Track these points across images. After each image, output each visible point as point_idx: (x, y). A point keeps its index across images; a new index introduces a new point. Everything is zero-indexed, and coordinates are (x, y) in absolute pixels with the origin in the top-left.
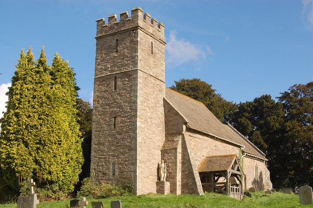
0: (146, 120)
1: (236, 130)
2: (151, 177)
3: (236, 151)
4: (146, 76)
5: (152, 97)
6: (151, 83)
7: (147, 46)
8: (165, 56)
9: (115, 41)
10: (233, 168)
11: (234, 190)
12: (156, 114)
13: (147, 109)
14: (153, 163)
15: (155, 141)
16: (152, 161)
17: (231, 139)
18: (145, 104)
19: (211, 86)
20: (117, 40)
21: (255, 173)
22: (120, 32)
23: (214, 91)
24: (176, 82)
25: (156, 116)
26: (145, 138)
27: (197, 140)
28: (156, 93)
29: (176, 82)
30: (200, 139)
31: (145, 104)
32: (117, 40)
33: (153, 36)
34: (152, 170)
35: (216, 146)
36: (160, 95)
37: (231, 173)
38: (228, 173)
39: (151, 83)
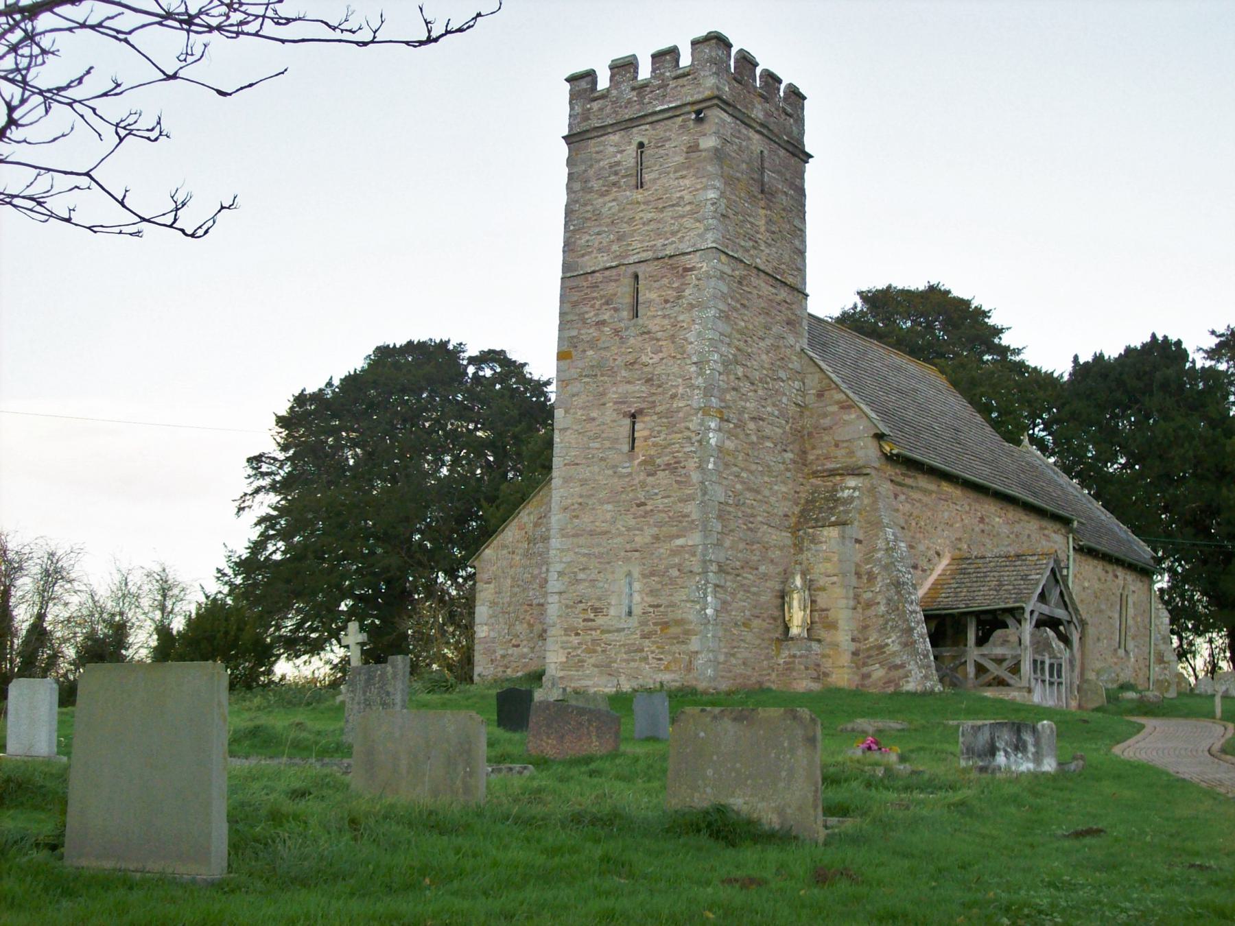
0: (741, 425)
1: (875, 342)
2: (756, 623)
3: (1057, 542)
4: (1148, 657)
5: (761, 344)
6: (760, 297)
7: (744, 166)
8: (325, 533)
9: (632, 149)
10: (1042, 597)
11: (1043, 669)
12: (774, 405)
13: (745, 387)
14: (765, 575)
15: (772, 500)
16: (762, 569)
17: (1035, 494)
18: (740, 371)
19: (1154, 336)
20: (641, 145)
21: (1117, 616)
22: (650, 119)
23: (997, 331)
24: (860, 293)
25: (776, 413)
26: (739, 486)
27: (916, 495)
28: (776, 329)
29: (860, 293)
30: (925, 491)
31: (740, 373)
32: (641, 145)
33: (765, 131)
34: (763, 599)
35: (982, 520)
36: (791, 340)
37: (1036, 615)
38: (1027, 615)
39: (760, 297)
